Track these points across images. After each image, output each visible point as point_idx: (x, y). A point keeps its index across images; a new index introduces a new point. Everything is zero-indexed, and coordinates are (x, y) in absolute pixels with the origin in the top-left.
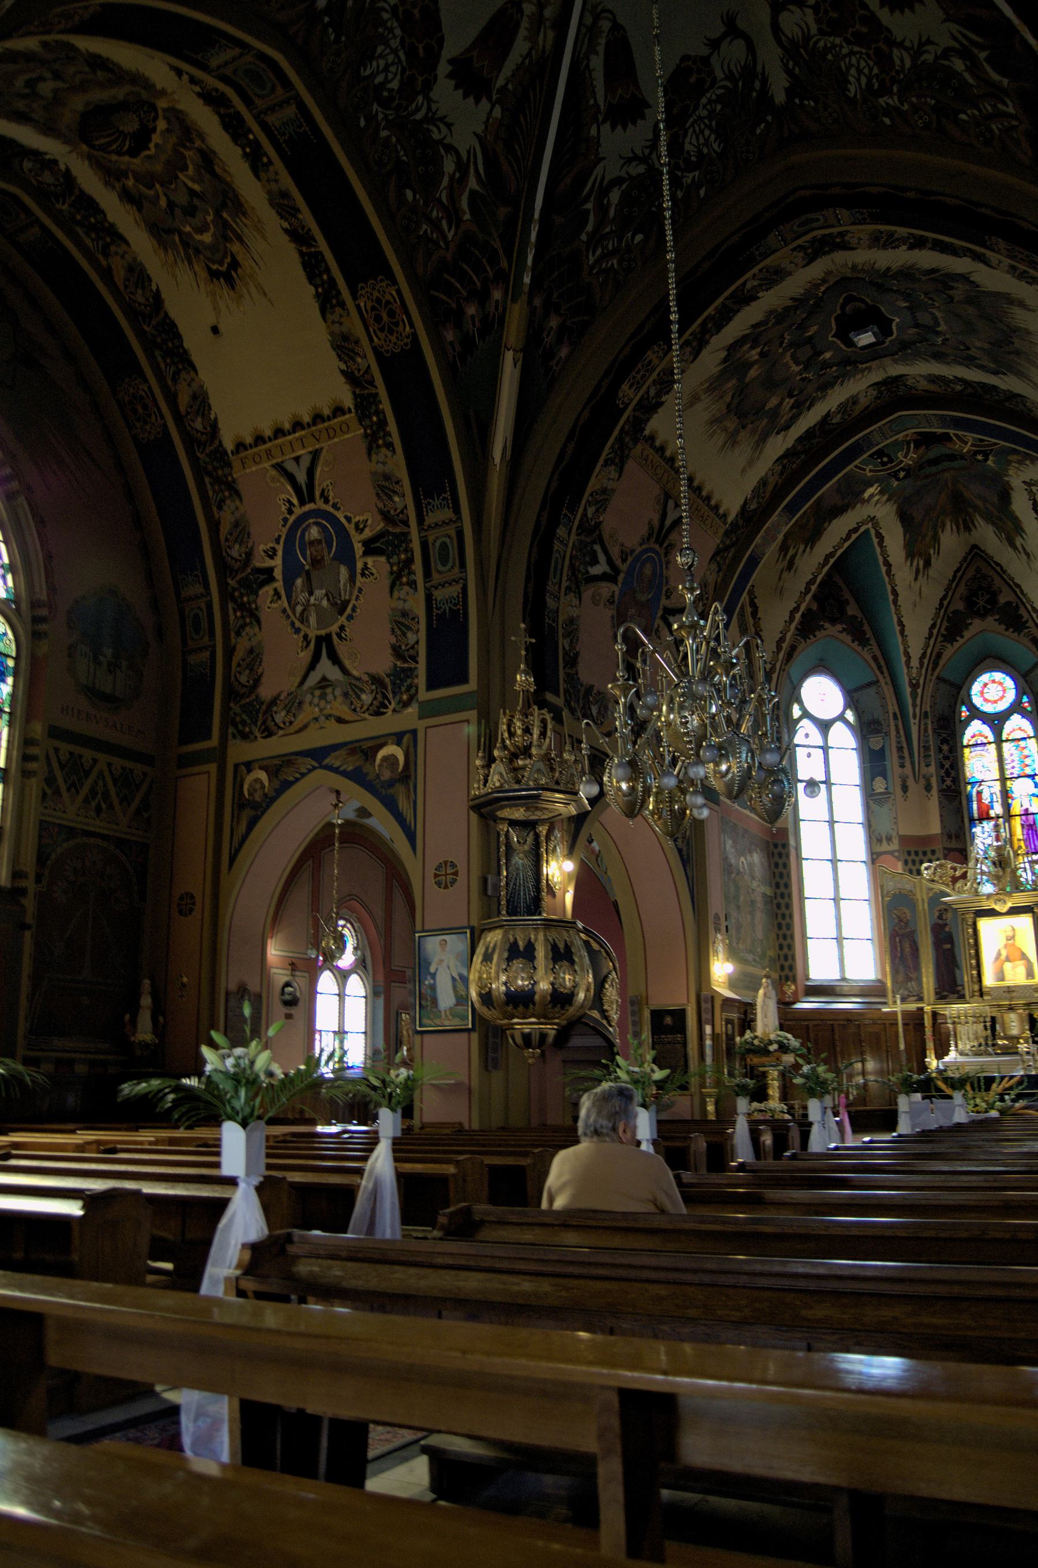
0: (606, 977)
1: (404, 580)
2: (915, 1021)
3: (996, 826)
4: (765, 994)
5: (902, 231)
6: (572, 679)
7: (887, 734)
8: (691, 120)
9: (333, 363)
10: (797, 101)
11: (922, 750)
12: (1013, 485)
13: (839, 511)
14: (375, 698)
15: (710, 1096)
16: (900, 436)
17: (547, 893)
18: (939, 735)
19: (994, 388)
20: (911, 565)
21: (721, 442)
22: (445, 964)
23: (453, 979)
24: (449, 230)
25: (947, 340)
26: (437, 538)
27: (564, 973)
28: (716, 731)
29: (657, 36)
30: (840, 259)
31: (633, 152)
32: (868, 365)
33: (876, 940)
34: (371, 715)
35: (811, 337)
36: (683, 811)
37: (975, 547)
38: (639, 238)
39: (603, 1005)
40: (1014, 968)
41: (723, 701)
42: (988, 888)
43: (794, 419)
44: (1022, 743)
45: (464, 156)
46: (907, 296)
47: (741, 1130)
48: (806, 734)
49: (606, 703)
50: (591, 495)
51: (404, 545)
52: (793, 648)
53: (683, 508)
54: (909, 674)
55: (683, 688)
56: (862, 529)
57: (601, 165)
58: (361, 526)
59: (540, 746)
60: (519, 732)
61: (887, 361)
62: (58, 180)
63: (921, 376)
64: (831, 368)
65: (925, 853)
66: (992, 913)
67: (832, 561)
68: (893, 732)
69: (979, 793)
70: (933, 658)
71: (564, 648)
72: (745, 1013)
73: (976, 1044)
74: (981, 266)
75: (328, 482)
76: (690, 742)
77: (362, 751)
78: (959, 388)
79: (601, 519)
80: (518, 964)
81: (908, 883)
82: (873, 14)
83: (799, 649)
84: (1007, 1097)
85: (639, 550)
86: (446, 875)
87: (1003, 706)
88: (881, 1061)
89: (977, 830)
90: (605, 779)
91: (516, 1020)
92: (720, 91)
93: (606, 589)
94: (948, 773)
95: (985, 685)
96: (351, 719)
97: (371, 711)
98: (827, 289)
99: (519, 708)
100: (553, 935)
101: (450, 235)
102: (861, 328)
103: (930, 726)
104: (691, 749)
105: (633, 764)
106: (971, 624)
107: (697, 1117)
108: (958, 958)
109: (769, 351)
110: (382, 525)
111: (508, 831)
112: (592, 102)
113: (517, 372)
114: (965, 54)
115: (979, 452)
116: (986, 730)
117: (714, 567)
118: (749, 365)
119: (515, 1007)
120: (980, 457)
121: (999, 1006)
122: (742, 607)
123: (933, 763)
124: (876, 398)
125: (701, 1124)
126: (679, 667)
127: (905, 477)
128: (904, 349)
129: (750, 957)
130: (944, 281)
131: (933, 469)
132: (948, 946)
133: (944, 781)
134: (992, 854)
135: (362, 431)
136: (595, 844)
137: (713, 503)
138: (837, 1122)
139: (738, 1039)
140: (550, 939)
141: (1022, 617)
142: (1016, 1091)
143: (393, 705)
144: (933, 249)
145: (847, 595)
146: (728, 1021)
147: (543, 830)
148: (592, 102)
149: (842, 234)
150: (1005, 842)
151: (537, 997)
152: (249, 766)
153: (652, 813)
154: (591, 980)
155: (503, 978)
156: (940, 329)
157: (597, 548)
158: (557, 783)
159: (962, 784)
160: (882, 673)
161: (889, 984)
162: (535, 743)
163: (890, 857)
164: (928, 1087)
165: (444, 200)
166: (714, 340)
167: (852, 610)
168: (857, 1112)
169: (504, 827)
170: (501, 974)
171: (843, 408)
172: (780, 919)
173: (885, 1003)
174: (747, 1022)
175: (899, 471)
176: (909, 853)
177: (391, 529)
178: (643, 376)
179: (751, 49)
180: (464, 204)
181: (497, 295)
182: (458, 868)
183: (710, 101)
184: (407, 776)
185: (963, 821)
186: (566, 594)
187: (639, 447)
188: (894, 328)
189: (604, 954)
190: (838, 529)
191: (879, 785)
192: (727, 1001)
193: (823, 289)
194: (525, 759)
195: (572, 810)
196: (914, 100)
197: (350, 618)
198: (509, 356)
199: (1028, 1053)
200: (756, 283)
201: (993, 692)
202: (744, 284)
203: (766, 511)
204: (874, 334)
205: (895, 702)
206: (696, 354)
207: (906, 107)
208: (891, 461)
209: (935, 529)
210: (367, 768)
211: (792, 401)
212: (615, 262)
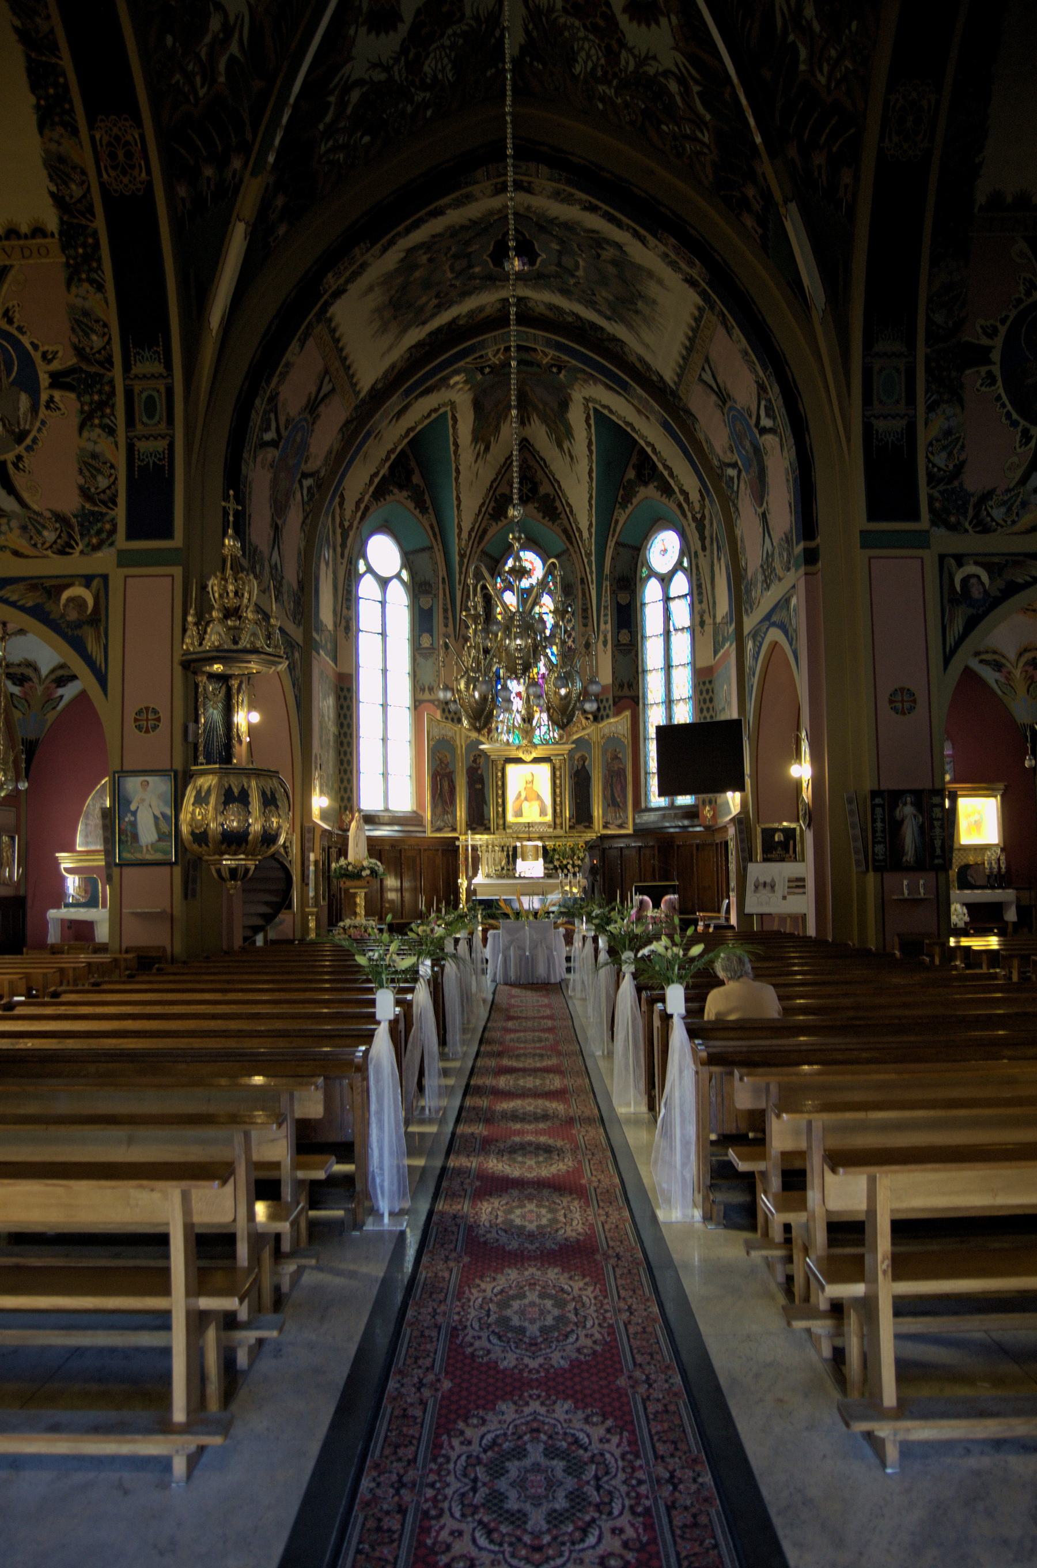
1: (97, 421)
7: (436, 596)
9: (41, 182)
10: (528, 59)
14: (59, 537)
15: (312, 914)
19: (602, 329)
22: (146, 804)
23: (156, 818)
24: (202, 86)
34: (54, 553)
35: (471, 253)
38: (367, 139)
43: (433, 316)
46: (562, 242)
48: (368, 587)
51: (98, 386)
52: (367, 508)
54: (459, 544)
56: (442, 411)
58: (50, 357)
60: (231, 595)
62: (947, 466)
66: (519, 761)
73: (499, 868)
74: (639, 245)
75: (15, 303)
77: (45, 588)
78: (570, 319)
80: (233, 807)
82: (613, 15)
83: (371, 510)
92: (465, 28)
96: (30, 553)
97: (55, 550)
101: (201, 93)
110: (74, 360)
114: (681, 81)
127: (489, 373)
130: (598, 242)
132: (479, 786)
135: (64, 260)
139: (333, 865)
141: (556, 508)
143: (81, 546)
145: (413, 464)
147: (235, 683)
149: (530, 183)
151: (250, 837)
152: (960, 560)
156: (577, 274)
160: (436, 540)
161: (428, 815)
163: (431, 705)
167: (416, 479)
171: (471, 314)
177: (84, 367)
180: (222, 66)
181: (237, 164)
182: (161, 714)
183: (455, 34)
184: (97, 618)
187: (320, 326)
191: (426, 641)
193: (496, 217)
197: (29, 449)
207: (619, 101)
210: (49, 606)
212: (342, 156)
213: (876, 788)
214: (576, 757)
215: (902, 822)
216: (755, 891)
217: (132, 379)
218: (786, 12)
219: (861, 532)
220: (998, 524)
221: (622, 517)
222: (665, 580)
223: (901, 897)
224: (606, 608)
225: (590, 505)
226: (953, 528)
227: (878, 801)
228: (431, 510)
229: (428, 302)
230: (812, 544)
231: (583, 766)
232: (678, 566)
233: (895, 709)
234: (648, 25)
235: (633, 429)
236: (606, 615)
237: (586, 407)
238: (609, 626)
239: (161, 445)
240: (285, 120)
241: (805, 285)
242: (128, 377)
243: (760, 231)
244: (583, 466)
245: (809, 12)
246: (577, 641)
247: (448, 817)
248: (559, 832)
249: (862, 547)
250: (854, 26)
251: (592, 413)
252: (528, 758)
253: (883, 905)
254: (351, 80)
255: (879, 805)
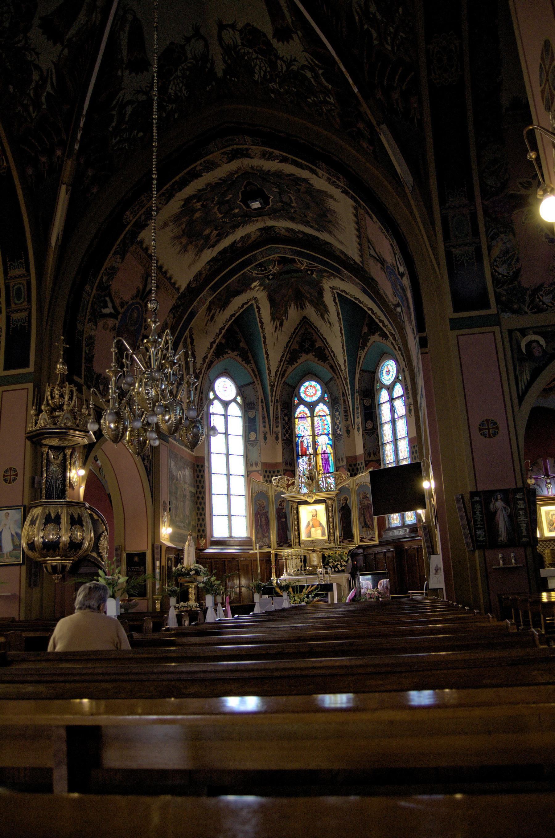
0: (101, 534)
2: (266, 558)
3: (310, 459)
4: (189, 544)
5: (277, 152)
6: (90, 369)
7: (257, 410)
8: (173, 77)
10: (228, 77)
11: (275, 419)
12: (325, 288)
13: (238, 293)
15: (158, 600)
16: (271, 257)
17: (70, 487)
18: (283, 411)
19: (318, 238)
20: (273, 324)
21: (178, 250)
23: (12, 535)
24: (34, 112)
25: (296, 211)
26: (15, 284)
27: (77, 531)
28: (164, 398)
29: (156, 27)
30: (246, 162)
31: (140, 87)
32: (257, 218)
33: (248, 516)
36: (145, 441)
37: (305, 318)
38: (141, 134)
39: (99, 550)
40: (315, 531)
41: (168, 382)
42: (304, 490)
43: (217, 242)
44: (324, 418)
45: (45, 73)
46: (278, 186)
47: (172, 614)
48: (216, 408)
49: (106, 381)
50: (106, 269)
52: (211, 362)
53: (153, 278)
55: (147, 374)
56: (250, 303)
57: (122, 92)
59: (69, 405)
61: (266, 218)
63: (283, 227)
64: (238, 218)
65: (274, 472)
66: (306, 503)
67: (234, 318)
68: (261, 409)
69: (302, 442)
70: (282, 372)
71: (85, 352)
72: (178, 555)
73: (296, 570)
74: (314, 176)
76: (150, 404)
78: (300, 236)
79: (110, 283)
80: (50, 526)
81: (265, 487)
82: (269, 40)
83: (214, 364)
84: (310, 596)
85: (130, 302)
86: (10, 476)
87: (315, 399)
88: (249, 579)
89: (300, 461)
90: (102, 421)
91: (48, 558)
93: (111, 322)
94: (287, 432)
95: (307, 387)
98: (238, 176)
99: (57, 383)
100: (72, 510)
101: (34, 115)
102: (254, 200)
103: (279, 407)
104: (150, 407)
105: (118, 414)
106: (301, 356)
107: (150, 610)
108: (288, 525)
109: (206, 204)
111: (48, 452)
112: (120, 57)
113: (68, 197)
114: (312, 70)
115: (309, 270)
116: (306, 410)
117: (171, 315)
118: (194, 211)
119: (48, 551)
120: (309, 272)
121: (308, 550)
122: (186, 339)
123: (280, 426)
124: (260, 236)
125: (153, 614)
126: (146, 363)
127: (272, 279)
128: (274, 213)
129: (182, 525)
130: (297, 181)
131: (286, 276)
132: (284, 520)
133: (285, 435)
134: (307, 473)
136: (99, 462)
137: (168, 275)
138: (224, 610)
139: (174, 568)
140: (70, 513)
141: (325, 354)
142: (315, 593)
144: (291, 164)
146: (169, 559)
147: (68, 452)
148: (120, 57)
149: (247, 149)
150: (313, 467)
151: (61, 545)
152: (523, 332)
153: (128, 442)
154: (92, 535)
155: (42, 534)
156: (293, 205)
157: (107, 299)
158: (78, 426)
159: (294, 437)
160: (256, 378)
162: (66, 403)
164: (270, 591)
165: (32, 95)
166: (178, 194)
167: (242, 345)
168: (236, 606)
169: (46, 449)
170: (40, 532)
171: (243, 239)
172: (199, 505)
173: (252, 549)
174: (179, 559)
175: (269, 275)
176: (266, 472)
178: (138, 208)
179: (207, 46)
181: (59, 153)
185: (293, 456)
186: (88, 323)
187: (134, 246)
188: (270, 201)
189: (100, 521)
190: (237, 303)
191: (253, 436)
192: (168, 548)
193: (236, 176)
194: (60, 411)
195: (86, 441)
196: (286, 87)
198: (63, 188)
199: (321, 574)
200: (201, 168)
201: (310, 391)
202: (195, 167)
203: (200, 290)
204: (261, 203)
205: (262, 394)
206: (168, 201)
207: (282, 90)
208: (266, 270)
209: (286, 306)
211: (217, 232)
213: (474, 490)
214: (342, 498)
215: (496, 512)
216: (435, 574)
217: (9, 279)
218: (358, 10)
219: (450, 319)
220: (548, 306)
221: (362, 354)
222: (390, 389)
223: (498, 567)
224: (357, 408)
225: (344, 350)
226: (515, 312)
227: (476, 499)
228: (252, 362)
229: (211, 233)
230: (424, 334)
231: (346, 504)
232: (396, 380)
233: (484, 435)
234: (288, 42)
235: (360, 301)
236: (358, 413)
237: (333, 292)
238: (360, 420)
239: (24, 314)
240: (82, 124)
241: (398, 172)
242: (7, 279)
243: (371, 148)
244: (337, 327)
245: (373, 8)
246: (342, 430)
247: (266, 539)
248: (332, 545)
249: (451, 329)
250: (401, 10)
251: (336, 296)
252: (311, 500)
253: (486, 575)
254: (124, 102)
255: (477, 502)
